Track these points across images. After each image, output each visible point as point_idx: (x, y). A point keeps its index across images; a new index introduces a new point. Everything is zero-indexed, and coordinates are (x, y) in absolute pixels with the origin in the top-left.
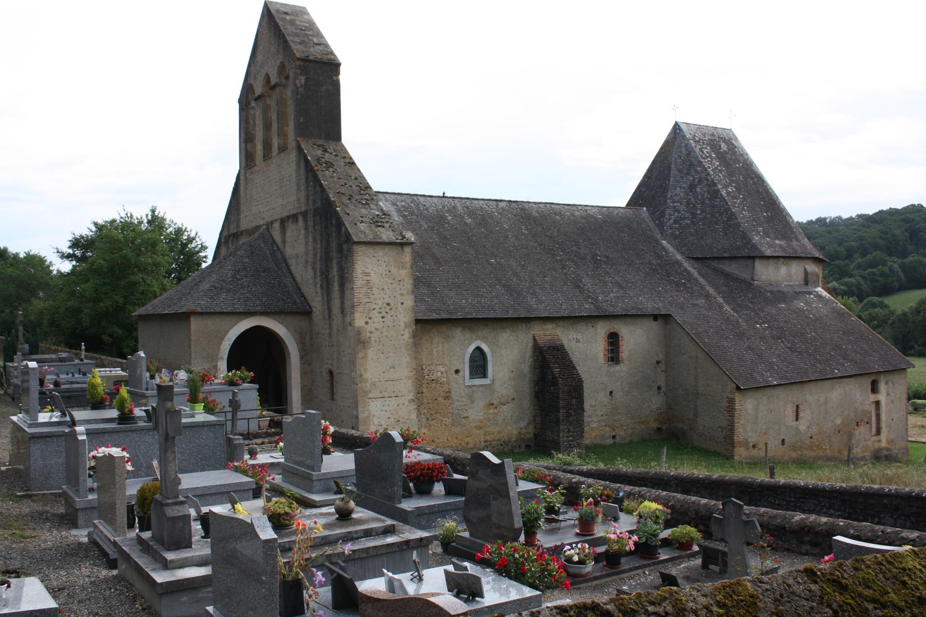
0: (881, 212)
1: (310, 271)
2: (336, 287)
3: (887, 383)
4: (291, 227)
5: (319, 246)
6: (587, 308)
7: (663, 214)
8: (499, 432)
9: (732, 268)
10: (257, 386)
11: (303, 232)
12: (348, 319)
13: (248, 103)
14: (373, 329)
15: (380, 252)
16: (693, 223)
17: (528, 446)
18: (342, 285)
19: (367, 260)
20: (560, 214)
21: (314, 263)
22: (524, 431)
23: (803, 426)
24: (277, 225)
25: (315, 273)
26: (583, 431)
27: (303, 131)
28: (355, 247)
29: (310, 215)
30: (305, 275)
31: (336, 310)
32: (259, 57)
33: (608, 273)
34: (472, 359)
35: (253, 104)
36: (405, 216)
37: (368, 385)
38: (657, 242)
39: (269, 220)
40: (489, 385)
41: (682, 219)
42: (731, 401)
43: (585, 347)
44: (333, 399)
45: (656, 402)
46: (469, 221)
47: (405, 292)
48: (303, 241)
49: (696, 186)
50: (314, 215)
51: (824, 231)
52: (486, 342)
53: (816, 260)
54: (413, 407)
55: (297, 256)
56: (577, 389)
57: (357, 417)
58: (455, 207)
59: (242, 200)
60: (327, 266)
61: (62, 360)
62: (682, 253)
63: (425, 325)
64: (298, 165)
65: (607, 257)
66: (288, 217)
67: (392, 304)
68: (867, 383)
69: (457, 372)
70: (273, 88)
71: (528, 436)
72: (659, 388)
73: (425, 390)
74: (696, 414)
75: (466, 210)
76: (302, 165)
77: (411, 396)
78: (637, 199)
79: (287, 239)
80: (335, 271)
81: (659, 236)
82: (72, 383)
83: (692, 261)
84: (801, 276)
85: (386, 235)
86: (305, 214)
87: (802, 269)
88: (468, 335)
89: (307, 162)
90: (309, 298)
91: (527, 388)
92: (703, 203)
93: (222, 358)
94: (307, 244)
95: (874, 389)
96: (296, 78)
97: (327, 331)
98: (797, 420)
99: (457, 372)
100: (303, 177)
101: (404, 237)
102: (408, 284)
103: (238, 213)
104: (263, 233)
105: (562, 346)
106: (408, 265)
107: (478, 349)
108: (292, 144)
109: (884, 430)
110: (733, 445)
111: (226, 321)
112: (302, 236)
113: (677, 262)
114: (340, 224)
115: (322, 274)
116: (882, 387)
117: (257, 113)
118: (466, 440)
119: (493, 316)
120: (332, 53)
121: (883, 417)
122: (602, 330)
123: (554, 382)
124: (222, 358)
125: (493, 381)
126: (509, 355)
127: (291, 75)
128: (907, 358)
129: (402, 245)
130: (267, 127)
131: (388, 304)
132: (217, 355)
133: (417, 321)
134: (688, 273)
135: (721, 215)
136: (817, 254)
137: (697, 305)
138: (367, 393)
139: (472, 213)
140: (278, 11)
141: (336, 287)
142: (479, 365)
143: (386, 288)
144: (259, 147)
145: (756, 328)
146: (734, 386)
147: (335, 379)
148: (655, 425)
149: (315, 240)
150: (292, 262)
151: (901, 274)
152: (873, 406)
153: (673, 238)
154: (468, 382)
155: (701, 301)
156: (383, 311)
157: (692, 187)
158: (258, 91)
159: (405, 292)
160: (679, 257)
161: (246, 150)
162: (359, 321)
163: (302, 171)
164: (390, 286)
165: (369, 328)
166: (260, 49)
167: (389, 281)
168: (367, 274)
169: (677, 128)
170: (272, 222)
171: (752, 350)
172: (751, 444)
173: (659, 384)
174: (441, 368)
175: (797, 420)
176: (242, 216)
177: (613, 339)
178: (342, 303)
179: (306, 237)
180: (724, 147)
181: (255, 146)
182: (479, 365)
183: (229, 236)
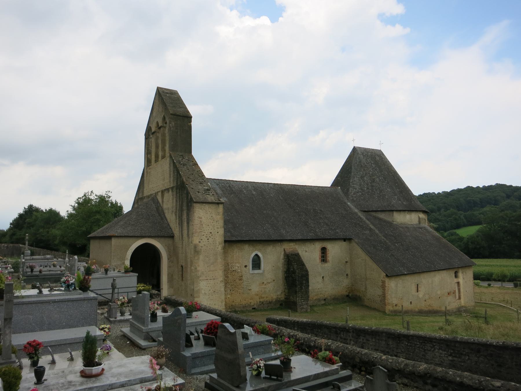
0: (453, 190)
1: (174, 216)
2: (185, 224)
3: (462, 273)
4: (166, 195)
5: (178, 204)
6: (311, 235)
7: (348, 190)
8: (267, 297)
9: (382, 216)
10: (137, 274)
11: (171, 197)
12: (190, 240)
13: (149, 135)
14: (203, 245)
15: (207, 206)
16: (362, 194)
17: (281, 305)
18: (188, 223)
19: (200, 210)
20: (299, 190)
21: (176, 212)
22: (279, 297)
23: (421, 294)
24: (160, 194)
25: (176, 217)
26: (308, 297)
27: (173, 148)
28: (195, 205)
29: (174, 189)
30: (171, 218)
31: (185, 235)
32: (154, 114)
33: (321, 218)
34: (253, 260)
35: (151, 136)
36: (223, 191)
37: (200, 273)
38: (345, 203)
39: (156, 191)
40: (262, 273)
41: (358, 192)
42: (383, 282)
43: (309, 254)
44: (182, 280)
45: (346, 282)
46: (254, 193)
47: (219, 227)
48: (171, 201)
49: (364, 177)
50: (177, 189)
51: (427, 197)
52: (260, 252)
53: (424, 212)
54: (222, 284)
55: (168, 209)
56: (305, 276)
57: (193, 289)
58: (247, 186)
59: (145, 182)
60: (181, 214)
61: (48, 259)
62: (358, 209)
63: (230, 242)
64: (170, 164)
65: (321, 210)
66: (165, 190)
67: (213, 233)
68: (452, 273)
69: (246, 266)
70: (160, 128)
71: (282, 299)
72: (347, 275)
73: (229, 276)
74: (366, 289)
75: (253, 188)
76: (172, 165)
77: (221, 279)
78: (337, 182)
79: (164, 200)
80: (185, 216)
81: (346, 201)
82: (50, 271)
83: (362, 212)
84: (417, 219)
85: (210, 198)
86: (172, 188)
87: (417, 216)
88: (251, 249)
89: (174, 163)
90: (173, 229)
91: (280, 275)
92: (367, 184)
93: (127, 259)
94: (173, 202)
95: (456, 276)
96: (170, 123)
97: (181, 246)
98: (417, 292)
99: (246, 266)
100: (172, 170)
101: (220, 201)
102: (221, 223)
103: (143, 188)
104: (153, 199)
105: (298, 254)
106: (221, 214)
107: (257, 255)
108: (167, 155)
109: (462, 297)
110: (385, 304)
111: (131, 240)
112: (171, 199)
113: (356, 213)
114: (188, 193)
115: (179, 217)
116: (460, 274)
117: (153, 140)
118: (250, 301)
119: (265, 239)
120: (188, 112)
121: (462, 290)
122: (318, 246)
123: (294, 272)
124: (127, 259)
125: (264, 271)
126: (272, 258)
127: (168, 122)
128: (472, 260)
129: (218, 204)
130: (157, 147)
131: (211, 233)
132: (125, 257)
133: (225, 241)
134: (361, 218)
135: (376, 190)
136: (424, 209)
137: (365, 234)
138: (199, 277)
139: (255, 189)
140: (163, 92)
141: (185, 224)
142: (257, 263)
143: (210, 225)
144: (153, 157)
145: (395, 246)
146: (385, 274)
147: (184, 270)
148: (347, 293)
149: (176, 201)
150: (166, 211)
151: (465, 220)
152: (456, 285)
153: (353, 201)
154: (251, 272)
155: (367, 232)
156: (210, 235)
157: (362, 177)
158: (153, 130)
159: (219, 227)
160: (356, 211)
161: (148, 158)
162: (196, 240)
163: (172, 167)
164: (212, 224)
165: (200, 245)
166: (155, 110)
167: (212, 221)
168: (201, 218)
169: (355, 149)
170: (158, 192)
171: (394, 256)
172: (394, 304)
173: (347, 273)
174: (238, 265)
175: (417, 292)
176: (145, 189)
177: (324, 250)
178: (188, 232)
179: (173, 199)
180: (378, 158)
181: (151, 157)
182: (257, 263)
183: (139, 199)
